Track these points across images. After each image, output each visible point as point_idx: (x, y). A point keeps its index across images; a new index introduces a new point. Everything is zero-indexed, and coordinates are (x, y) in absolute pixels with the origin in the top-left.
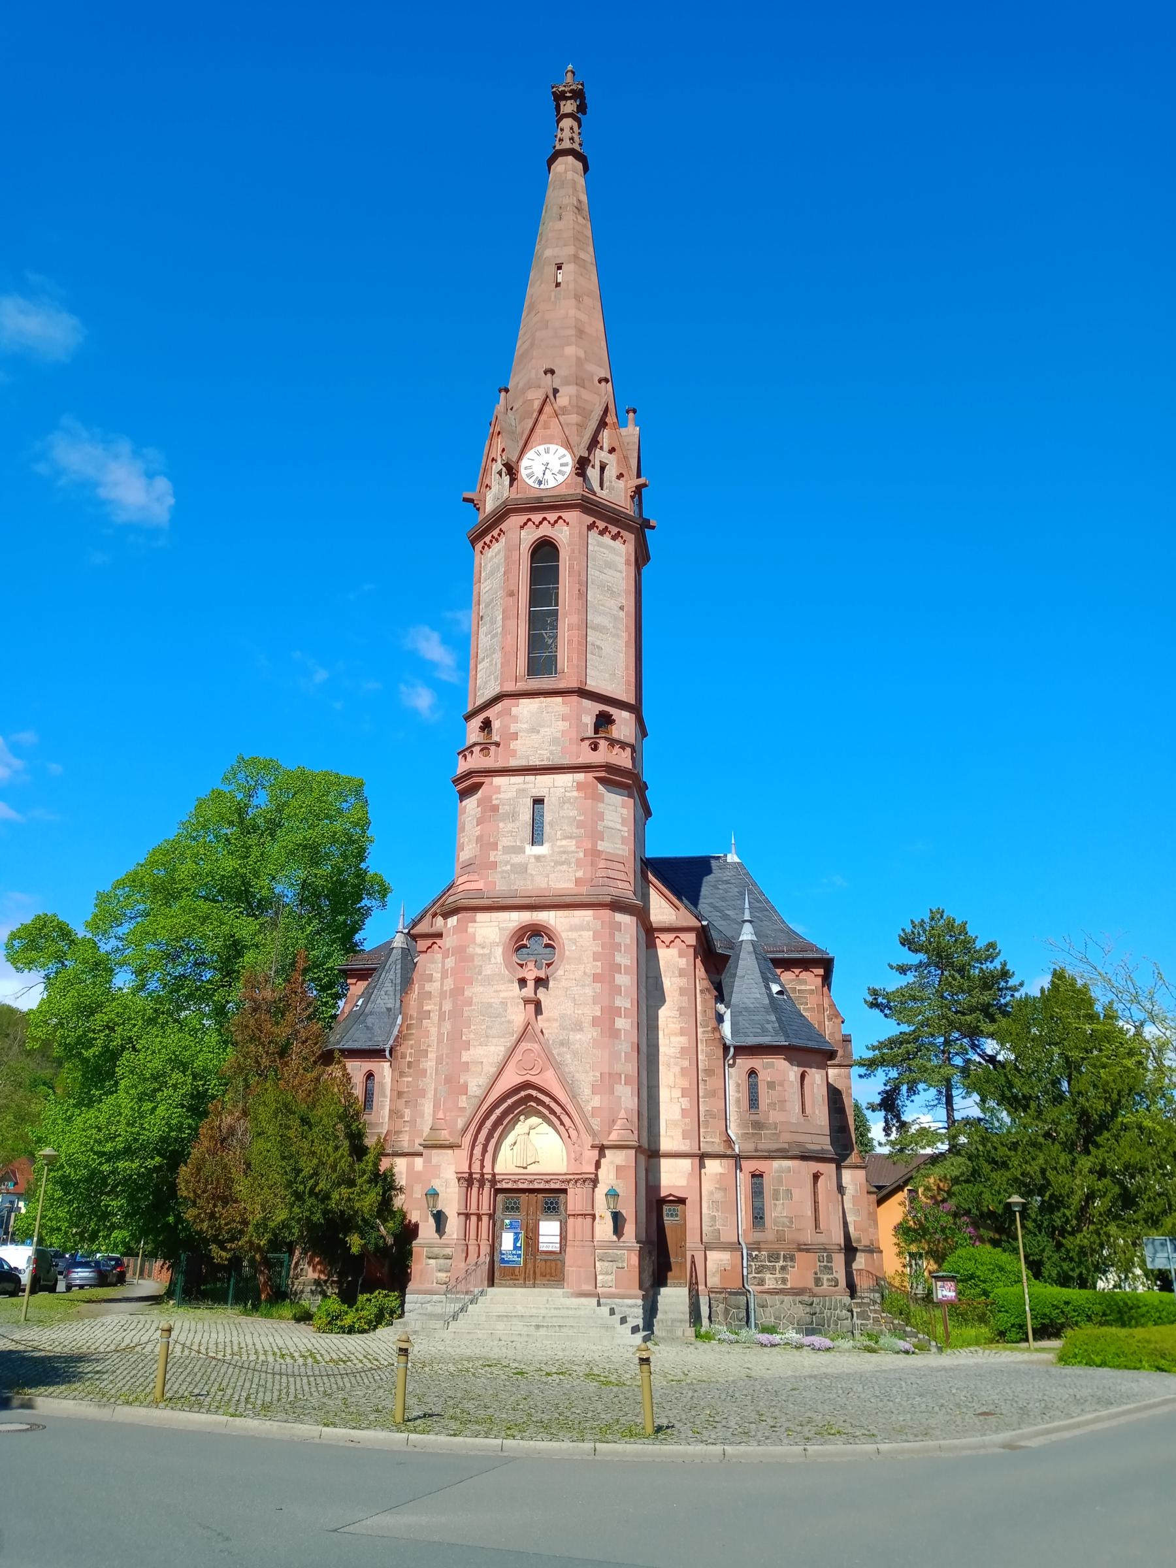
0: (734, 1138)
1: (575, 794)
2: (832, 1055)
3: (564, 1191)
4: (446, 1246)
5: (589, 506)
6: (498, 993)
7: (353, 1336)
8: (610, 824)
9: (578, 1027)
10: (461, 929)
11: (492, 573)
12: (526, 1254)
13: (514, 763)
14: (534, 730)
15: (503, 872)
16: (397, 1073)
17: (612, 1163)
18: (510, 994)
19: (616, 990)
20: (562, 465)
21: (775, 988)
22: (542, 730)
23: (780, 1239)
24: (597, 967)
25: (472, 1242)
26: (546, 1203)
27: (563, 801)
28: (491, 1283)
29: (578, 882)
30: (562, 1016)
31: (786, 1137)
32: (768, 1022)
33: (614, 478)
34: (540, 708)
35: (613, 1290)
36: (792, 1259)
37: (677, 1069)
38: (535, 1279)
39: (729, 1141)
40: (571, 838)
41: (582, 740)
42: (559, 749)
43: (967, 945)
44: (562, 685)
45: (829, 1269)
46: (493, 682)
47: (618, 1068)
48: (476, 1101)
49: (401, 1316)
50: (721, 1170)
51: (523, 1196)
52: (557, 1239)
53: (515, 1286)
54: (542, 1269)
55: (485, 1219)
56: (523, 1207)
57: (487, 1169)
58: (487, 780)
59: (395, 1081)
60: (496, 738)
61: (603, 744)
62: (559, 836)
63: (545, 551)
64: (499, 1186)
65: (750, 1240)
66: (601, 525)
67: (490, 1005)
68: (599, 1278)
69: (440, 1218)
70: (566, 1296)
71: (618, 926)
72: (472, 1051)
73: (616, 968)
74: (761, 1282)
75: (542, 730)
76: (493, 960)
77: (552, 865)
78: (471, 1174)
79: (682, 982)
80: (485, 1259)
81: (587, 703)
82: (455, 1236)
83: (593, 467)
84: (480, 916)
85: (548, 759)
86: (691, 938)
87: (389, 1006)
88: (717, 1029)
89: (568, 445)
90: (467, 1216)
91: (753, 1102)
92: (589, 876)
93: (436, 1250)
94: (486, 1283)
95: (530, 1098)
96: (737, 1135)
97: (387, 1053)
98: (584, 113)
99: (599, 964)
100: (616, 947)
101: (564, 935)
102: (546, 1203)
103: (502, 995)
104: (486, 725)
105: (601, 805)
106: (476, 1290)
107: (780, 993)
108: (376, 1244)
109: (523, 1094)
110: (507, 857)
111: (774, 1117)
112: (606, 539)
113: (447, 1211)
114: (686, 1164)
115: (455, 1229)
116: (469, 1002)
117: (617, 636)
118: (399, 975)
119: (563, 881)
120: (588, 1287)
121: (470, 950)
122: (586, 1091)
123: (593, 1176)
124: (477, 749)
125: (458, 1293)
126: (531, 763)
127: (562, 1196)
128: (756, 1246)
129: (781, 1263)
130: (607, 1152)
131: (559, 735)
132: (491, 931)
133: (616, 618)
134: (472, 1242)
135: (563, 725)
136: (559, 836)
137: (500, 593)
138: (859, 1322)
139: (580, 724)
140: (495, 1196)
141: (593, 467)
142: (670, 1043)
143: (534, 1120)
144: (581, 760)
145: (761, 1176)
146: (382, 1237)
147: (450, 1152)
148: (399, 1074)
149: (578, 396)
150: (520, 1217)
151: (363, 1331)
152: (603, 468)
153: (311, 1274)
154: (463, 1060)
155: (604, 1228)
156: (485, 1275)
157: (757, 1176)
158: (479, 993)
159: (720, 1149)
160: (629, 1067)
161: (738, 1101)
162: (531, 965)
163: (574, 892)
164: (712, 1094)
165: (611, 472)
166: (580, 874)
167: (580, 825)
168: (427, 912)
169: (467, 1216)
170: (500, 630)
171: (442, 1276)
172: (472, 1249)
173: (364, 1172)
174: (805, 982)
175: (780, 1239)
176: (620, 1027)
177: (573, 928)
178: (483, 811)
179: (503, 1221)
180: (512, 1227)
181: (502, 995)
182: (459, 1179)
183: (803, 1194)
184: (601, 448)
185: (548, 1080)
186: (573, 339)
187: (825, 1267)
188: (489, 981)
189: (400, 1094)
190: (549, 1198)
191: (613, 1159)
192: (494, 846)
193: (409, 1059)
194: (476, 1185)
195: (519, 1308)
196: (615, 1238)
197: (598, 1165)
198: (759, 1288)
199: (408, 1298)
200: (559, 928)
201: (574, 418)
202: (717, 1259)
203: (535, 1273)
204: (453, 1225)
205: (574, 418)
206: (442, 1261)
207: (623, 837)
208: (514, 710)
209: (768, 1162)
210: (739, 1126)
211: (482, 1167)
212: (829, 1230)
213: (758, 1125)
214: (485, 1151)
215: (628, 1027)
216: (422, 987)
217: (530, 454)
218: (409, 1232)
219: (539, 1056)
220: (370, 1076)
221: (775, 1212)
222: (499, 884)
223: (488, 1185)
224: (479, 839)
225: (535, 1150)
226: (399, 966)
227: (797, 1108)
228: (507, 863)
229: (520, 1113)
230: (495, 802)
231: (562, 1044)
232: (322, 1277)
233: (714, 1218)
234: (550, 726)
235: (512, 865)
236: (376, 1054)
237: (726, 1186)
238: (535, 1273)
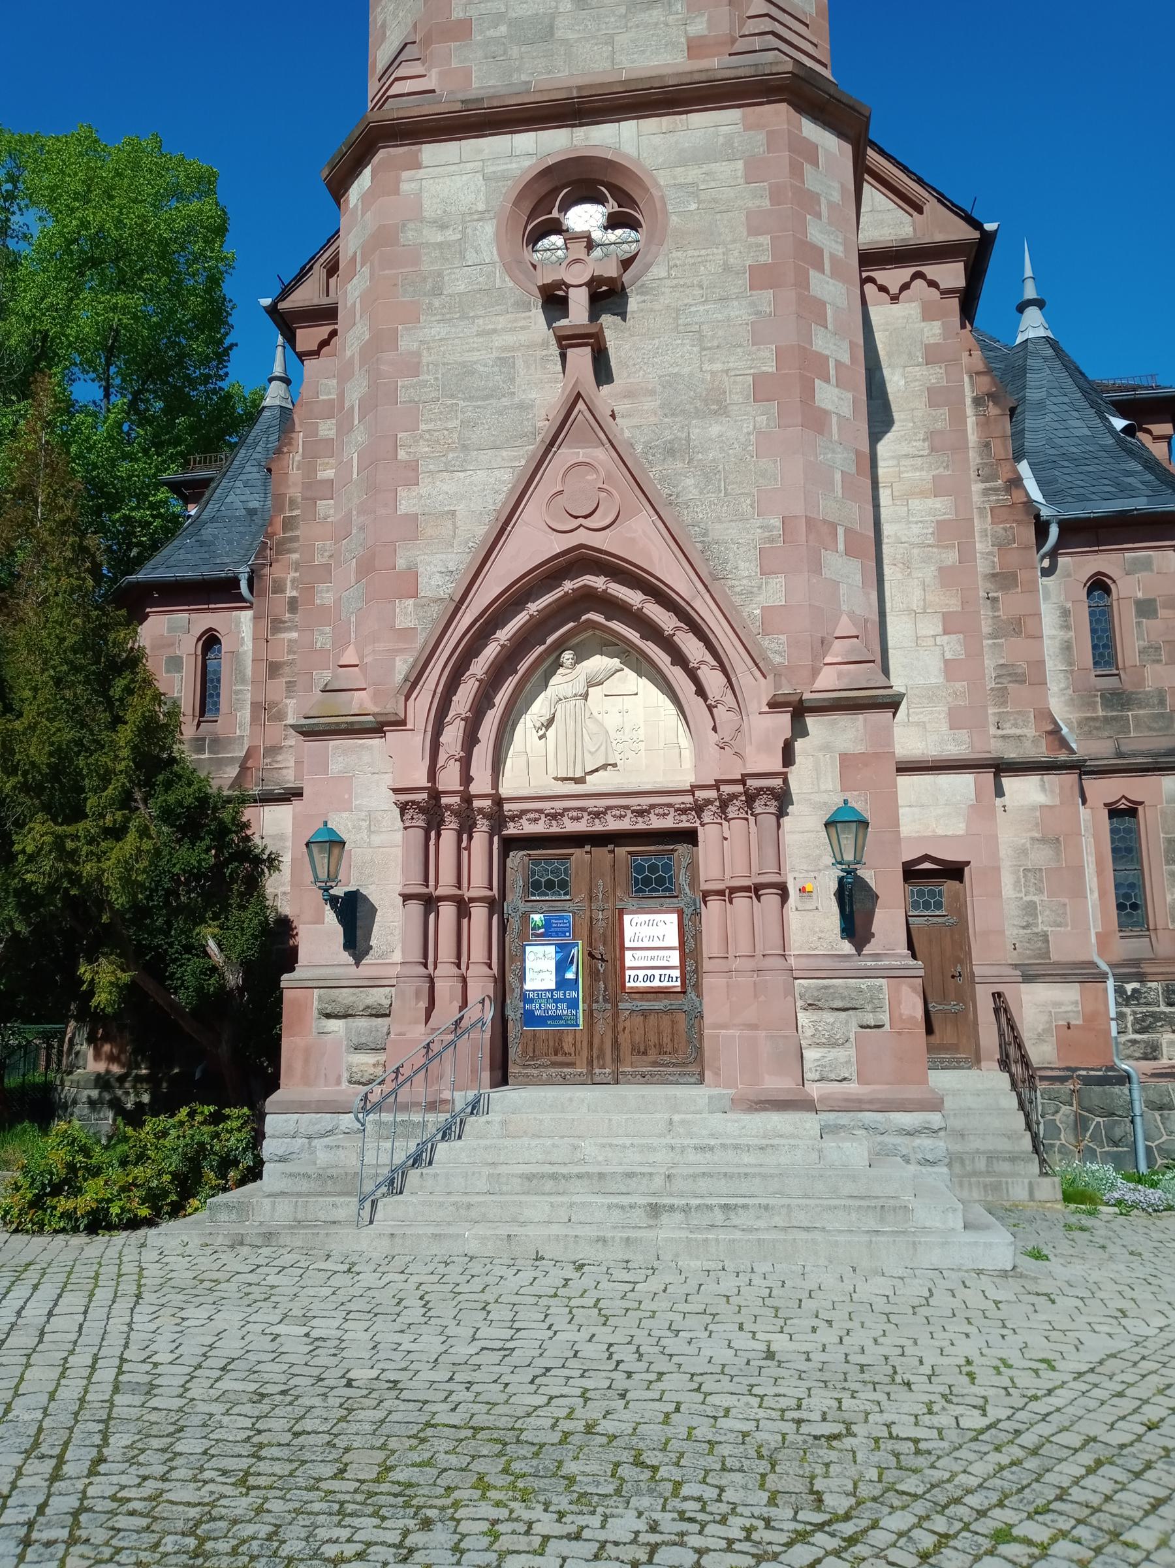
3: (690, 837)
4: (374, 983)
7: (101, 1239)
9: (715, 404)
12: (591, 998)
16: (265, 623)
17: (826, 748)
18: (523, 337)
24: (762, 250)
25: (445, 970)
26: (639, 869)
28: (501, 1078)
29: (695, 47)
32: (1129, 473)
35: (853, 1088)
37: (929, 573)
38: (617, 1060)
48: (437, 613)
49: (254, 1173)
50: (1040, 798)
51: (578, 855)
52: (674, 958)
53: (565, 1081)
54: (654, 1038)
55: (479, 912)
56: (579, 886)
57: (481, 784)
59: (262, 640)
64: (511, 830)
67: (468, 370)
68: (810, 1055)
69: (353, 913)
71: (810, 153)
72: (424, 489)
78: (435, 795)
79: (935, 375)
80: (482, 1012)
82: (397, 957)
84: (430, 152)
87: (251, 505)
90: (430, 903)
91: (1104, 649)
92: (724, 29)
93: (345, 997)
94: (486, 1076)
97: (244, 585)
99: (766, 240)
102: (639, 869)
106: (461, 1099)
108: (200, 990)
109: (568, 586)
113: (372, 892)
115: (396, 939)
116: (413, 368)
120: (778, 1084)
121: (409, 235)
122: (742, 569)
123: (777, 782)
125: (405, 1107)
127: (682, 849)
128: (1131, 970)
130: (811, 721)
134: (445, 970)
140: (504, 856)
143: (598, 663)
145: (1132, 812)
146: (214, 969)
147: (375, 742)
150: (570, 907)
151: (134, 1224)
153: (93, 1066)
154: (404, 507)
155: (814, 923)
156: (484, 1056)
157: (1123, 814)
159: (1040, 751)
161: (1067, 648)
163: (688, 69)
166: (699, 27)
168: (313, 259)
169: (430, 903)
171: (365, 1062)
172: (446, 988)
173: (106, 777)
176: (829, 407)
177: (685, 159)
179: (525, 917)
180: (547, 933)
181: (498, 341)
182: (403, 808)
185: (638, 540)
189: (274, 669)
190: (649, 852)
193: (290, 592)
195: (589, 1148)
196: (847, 947)
197: (788, 757)
199: (272, 1123)
200: (648, 162)
203: (616, 1044)
204: (393, 929)
206: (362, 1023)
209: (1150, 780)
210: (1071, 702)
211: (467, 779)
213: (1118, 699)
214: (471, 740)
215: (846, 410)
218: (276, 947)
220: (210, 641)
223: (482, 825)
225: (605, 733)
229: (560, 646)
231: (671, 452)
232: (116, 1069)
233: (1030, 909)
236: (219, 591)
237: (1054, 836)
238: (616, 1044)
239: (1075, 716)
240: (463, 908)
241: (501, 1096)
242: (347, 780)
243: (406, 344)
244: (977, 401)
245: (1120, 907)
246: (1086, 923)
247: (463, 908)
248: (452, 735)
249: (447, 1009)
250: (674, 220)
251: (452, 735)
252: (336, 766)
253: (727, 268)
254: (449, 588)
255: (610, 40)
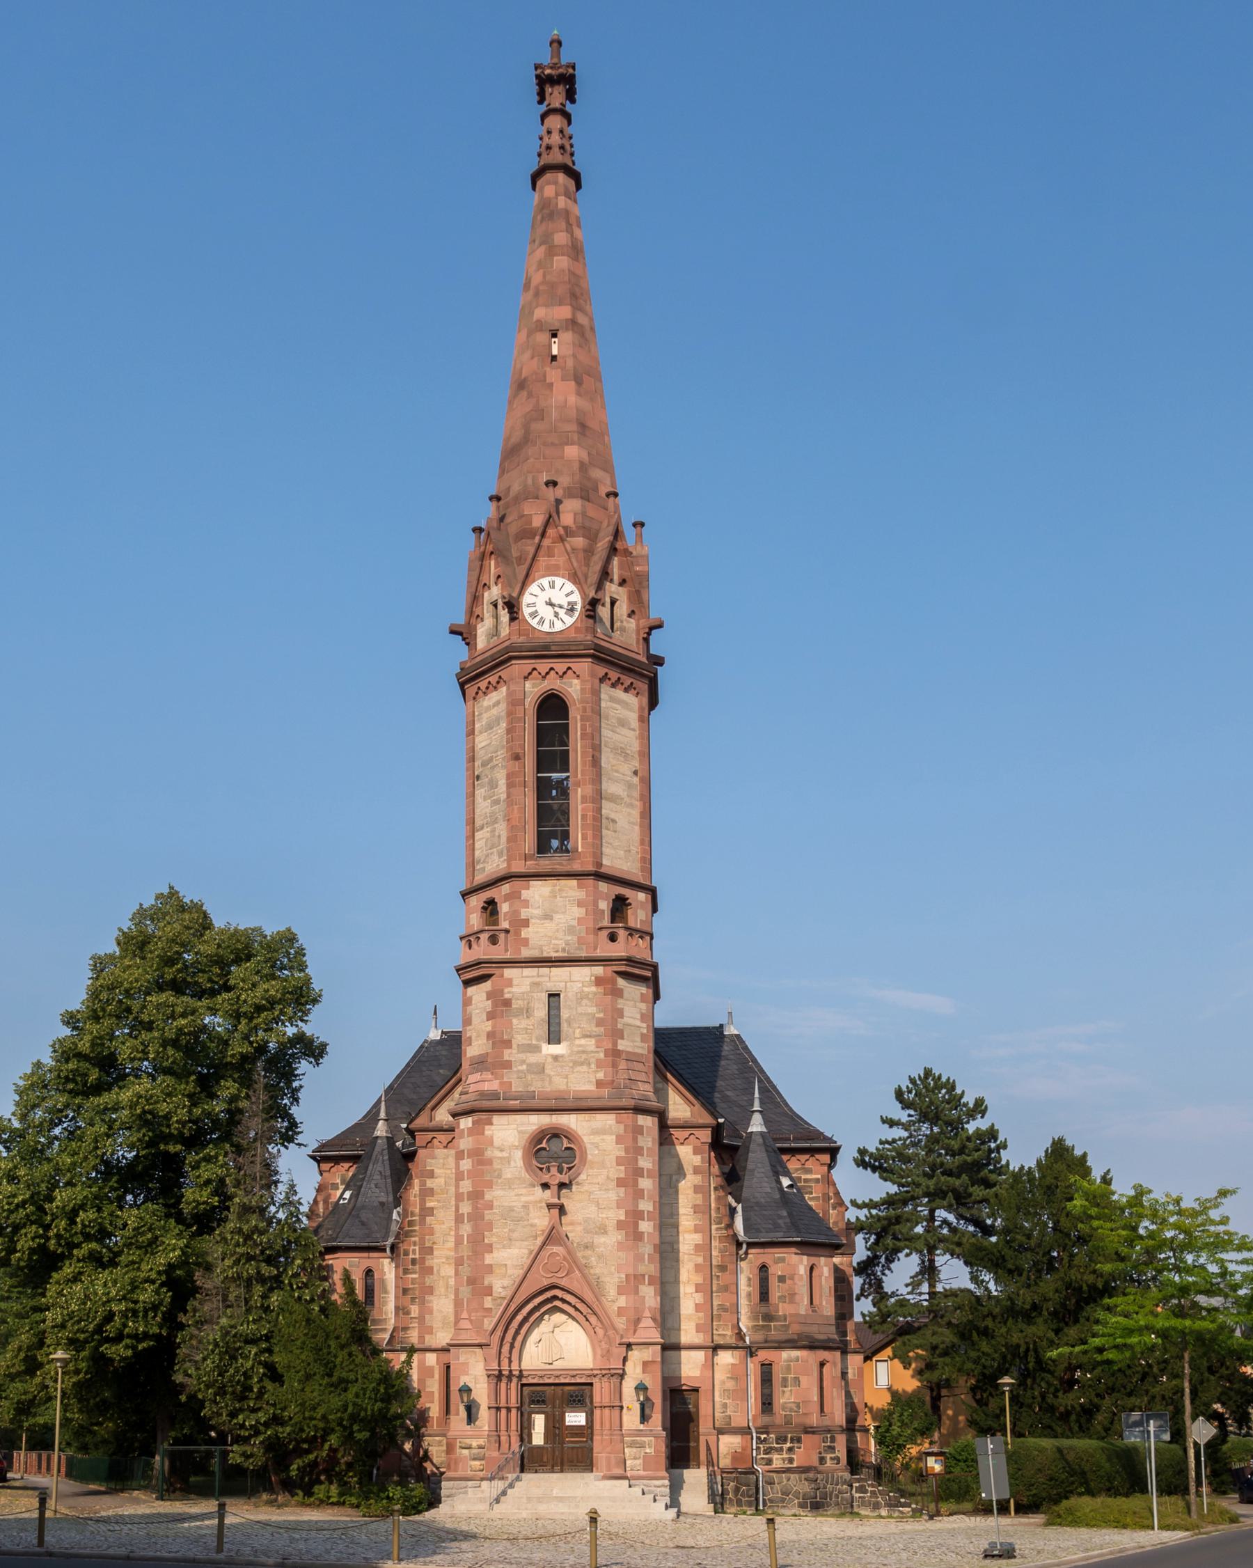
0: (745, 1330)
1: (594, 989)
2: (837, 1247)
3: (591, 1384)
5: (603, 656)
6: (518, 1196)
8: (630, 1021)
9: (603, 1230)
10: (477, 1130)
11: (489, 727)
13: (526, 953)
14: (547, 917)
15: (519, 1071)
18: (531, 1198)
19: (639, 1194)
20: (567, 595)
21: (786, 1182)
22: (556, 917)
23: (788, 1422)
24: (621, 1172)
27: (581, 997)
28: (522, 1471)
29: (599, 1084)
30: (586, 1220)
31: (795, 1329)
32: (780, 1217)
33: (625, 617)
34: (552, 892)
35: (642, 1473)
36: (799, 1440)
39: (740, 1335)
40: (590, 1036)
41: (600, 929)
42: (575, 938)
43: (955, 1100)
44: (576, 867)
45: (832, 1449)
46: (495, 857)
47: (642, 1269)
55: (514, 1411)
58: (497, 972)
60: (505, 925)
61: (622, 934)
62: (577, 1035)
63: (552, 708)
64: (524, 1381)
65: (759, 1424)
66: (614, 675)
67: (511, 1209)
68: (628, 1463)
70: (597, 1479)
71: (638, 1130)
72: (495, 1254)
73: (639, 1172)
74: (769, 1462)
75: (556, 917)
76: (513, 1164)
77: (571, 1065)
78: (500, 1371)
81: (603, 886)
83: (603, 605)
85: (564, 950)
86: (706, 1136)
88: (730, 1226)
89: (574, 578)
90: (498, 1409)
91: (764, 1295)
95: (555, 1298)
96: (748, 1328)
98: (573, 101)
99: (622, 1168)
100: (638, 1151)
101: (585, 1139)
103: (524, 1199)
104: (491, 907)
105: (620, 1001)
107: (790, 1186)
109: (548, 1295)
110: (522, 1056)
111: (783, 1309)
112: (619, 693)
114: (700, 1356)
116: (490, 1206)
117: (631, 806)
118: (388, 1167)
119: (583, 1082)
122: (612, 1291)
124: (484, 937)
126: (545, 955)
128: (764, 1429)
129: (789, 1445)
131: (575, 923)
132: (510, 1133)
133: (630, 786)
134: (503, 1433)
135: (579, 912)
136: (577, 1035)
137: (502, 754)
138: (857, 1495)
139: (598, 913)
141: (603, 605)
142: (688, 1240)
143: (558, 1317)
144: (599, 953)
148: (402, 1271)
149: (584, 514)
152: (613, 602)
154: (487, 1262)
155: (631, 1419)
158: (499, 1196)
160: (650, 1268)
161: (749, 1295)
162: (554, 1170)
164: (725, 1289)
165: (622, 609)
166: (600, 1075)
167: (600, 1023)
169: (498, 1409)
170: (503, 796)
174: (809, 1171)
175: (788, 1422)
177: (595, 1132)
178: (495, 1005)
183: (809, 1383)
184: (611, 581)
186: (575, 437)
187: (830, 1447)
188: (509, 1185)
189: (405, 1291)
190: (576, 1392)
191: (636, 1356)
192: (508, 1044)
193: (411, 1256)
194: (504, 1380)
197: (625, 1359)
198: (767, 1468)
200: (580, 1133)
201: (579, 542)
202: (729, 1444)
204: (484, 1414)
205: (579, 542)
207: (642, 1035)
208: (525, 894)
210: (749, 1318)
211: (510, 1362)
212: (832, 1413)
213: (768, 1317)
215: (651, 1230)
216: (423, 1184)
217: (533, 588)
219: (565, 1259)
220: (369, 1272)
221: (784, 1398)
222: (516, 1082)
223: (515, 1380)
224: (490, 1035)
225: (560, 1346)
226: (386, 1157)
227: (806, 1301)
228: (523, 1062)
230: (507, 996)
233: (725, 1406)
234: (564, 913)
235: (528, 1065)
237: (737, 1374)
239: (750, 1324)
240: (509, 1409)
241: (523, 1475)
242: (466, 1364)
243: (488, 1197)
244: (716, 1189)
245: (763, 1404)
246: (748, 1411)
247: (509, 1409)
248: (506, 1348)
249: (505, 1445)
250: (589, 1157)
251: (506, 1348)
252: (462, 1359)
253: (608, 1178)
254: (509, 1293)
255: (567, 1077)
